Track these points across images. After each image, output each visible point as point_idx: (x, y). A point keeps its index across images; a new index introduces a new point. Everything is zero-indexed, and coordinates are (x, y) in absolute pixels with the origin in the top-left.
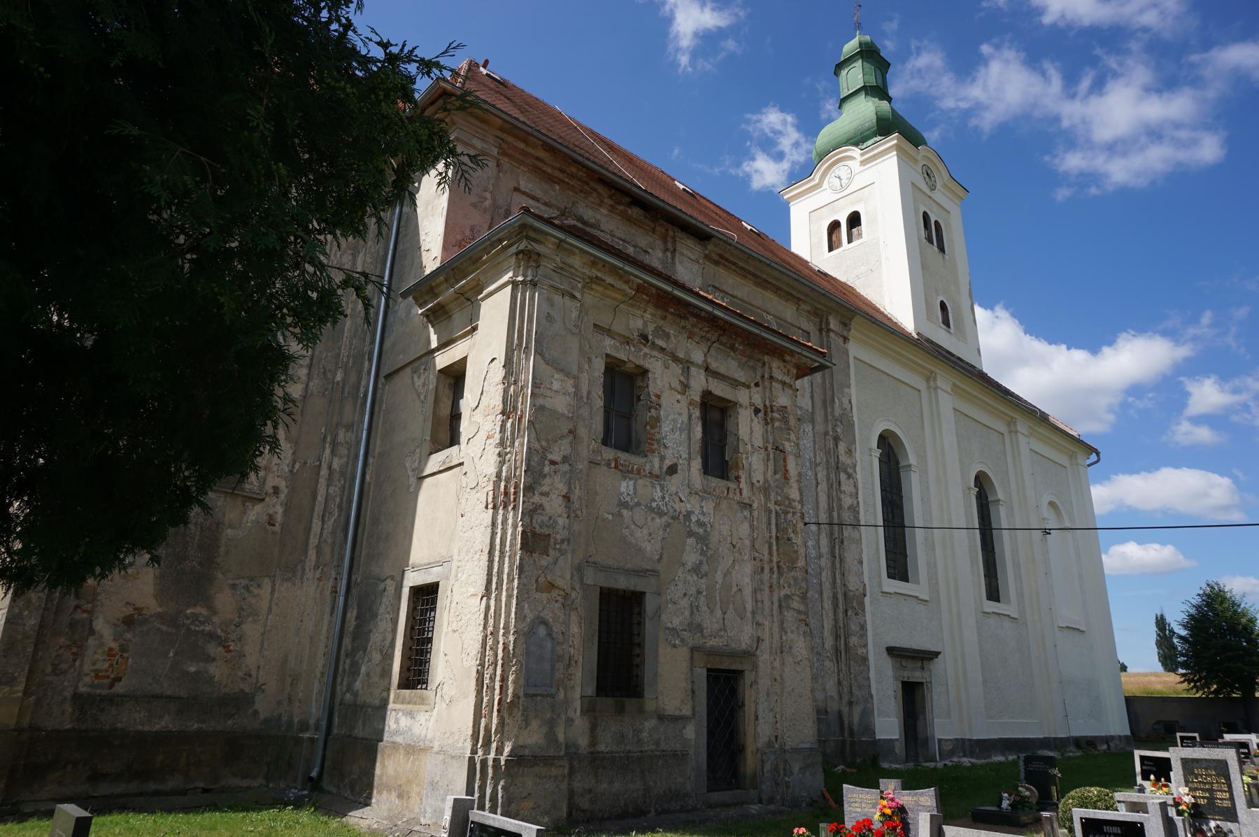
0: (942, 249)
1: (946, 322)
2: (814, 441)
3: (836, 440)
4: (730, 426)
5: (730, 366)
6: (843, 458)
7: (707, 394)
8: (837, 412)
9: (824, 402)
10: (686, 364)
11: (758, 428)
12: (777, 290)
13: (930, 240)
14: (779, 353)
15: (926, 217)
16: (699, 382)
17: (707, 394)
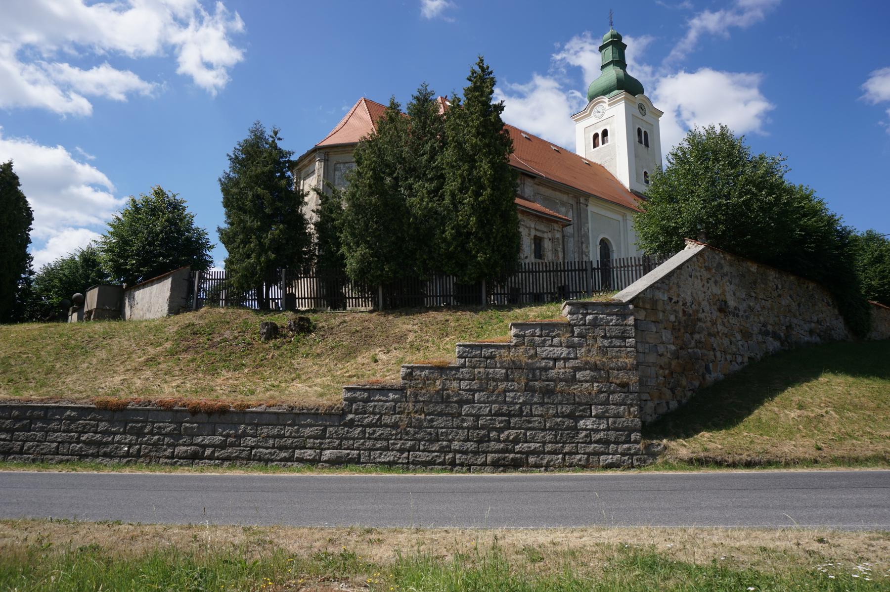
0: (647, 145)
2: (790, 296)
3: (582, 243)
5: (542, 227)
7: (535, 236)
10: (529, 228)
11: (550, 244)
12: (560, 191)
13: (640, 142)
14: (557, 222)
15: (639, 130)
16: (533, 233)
17: (535, 236)
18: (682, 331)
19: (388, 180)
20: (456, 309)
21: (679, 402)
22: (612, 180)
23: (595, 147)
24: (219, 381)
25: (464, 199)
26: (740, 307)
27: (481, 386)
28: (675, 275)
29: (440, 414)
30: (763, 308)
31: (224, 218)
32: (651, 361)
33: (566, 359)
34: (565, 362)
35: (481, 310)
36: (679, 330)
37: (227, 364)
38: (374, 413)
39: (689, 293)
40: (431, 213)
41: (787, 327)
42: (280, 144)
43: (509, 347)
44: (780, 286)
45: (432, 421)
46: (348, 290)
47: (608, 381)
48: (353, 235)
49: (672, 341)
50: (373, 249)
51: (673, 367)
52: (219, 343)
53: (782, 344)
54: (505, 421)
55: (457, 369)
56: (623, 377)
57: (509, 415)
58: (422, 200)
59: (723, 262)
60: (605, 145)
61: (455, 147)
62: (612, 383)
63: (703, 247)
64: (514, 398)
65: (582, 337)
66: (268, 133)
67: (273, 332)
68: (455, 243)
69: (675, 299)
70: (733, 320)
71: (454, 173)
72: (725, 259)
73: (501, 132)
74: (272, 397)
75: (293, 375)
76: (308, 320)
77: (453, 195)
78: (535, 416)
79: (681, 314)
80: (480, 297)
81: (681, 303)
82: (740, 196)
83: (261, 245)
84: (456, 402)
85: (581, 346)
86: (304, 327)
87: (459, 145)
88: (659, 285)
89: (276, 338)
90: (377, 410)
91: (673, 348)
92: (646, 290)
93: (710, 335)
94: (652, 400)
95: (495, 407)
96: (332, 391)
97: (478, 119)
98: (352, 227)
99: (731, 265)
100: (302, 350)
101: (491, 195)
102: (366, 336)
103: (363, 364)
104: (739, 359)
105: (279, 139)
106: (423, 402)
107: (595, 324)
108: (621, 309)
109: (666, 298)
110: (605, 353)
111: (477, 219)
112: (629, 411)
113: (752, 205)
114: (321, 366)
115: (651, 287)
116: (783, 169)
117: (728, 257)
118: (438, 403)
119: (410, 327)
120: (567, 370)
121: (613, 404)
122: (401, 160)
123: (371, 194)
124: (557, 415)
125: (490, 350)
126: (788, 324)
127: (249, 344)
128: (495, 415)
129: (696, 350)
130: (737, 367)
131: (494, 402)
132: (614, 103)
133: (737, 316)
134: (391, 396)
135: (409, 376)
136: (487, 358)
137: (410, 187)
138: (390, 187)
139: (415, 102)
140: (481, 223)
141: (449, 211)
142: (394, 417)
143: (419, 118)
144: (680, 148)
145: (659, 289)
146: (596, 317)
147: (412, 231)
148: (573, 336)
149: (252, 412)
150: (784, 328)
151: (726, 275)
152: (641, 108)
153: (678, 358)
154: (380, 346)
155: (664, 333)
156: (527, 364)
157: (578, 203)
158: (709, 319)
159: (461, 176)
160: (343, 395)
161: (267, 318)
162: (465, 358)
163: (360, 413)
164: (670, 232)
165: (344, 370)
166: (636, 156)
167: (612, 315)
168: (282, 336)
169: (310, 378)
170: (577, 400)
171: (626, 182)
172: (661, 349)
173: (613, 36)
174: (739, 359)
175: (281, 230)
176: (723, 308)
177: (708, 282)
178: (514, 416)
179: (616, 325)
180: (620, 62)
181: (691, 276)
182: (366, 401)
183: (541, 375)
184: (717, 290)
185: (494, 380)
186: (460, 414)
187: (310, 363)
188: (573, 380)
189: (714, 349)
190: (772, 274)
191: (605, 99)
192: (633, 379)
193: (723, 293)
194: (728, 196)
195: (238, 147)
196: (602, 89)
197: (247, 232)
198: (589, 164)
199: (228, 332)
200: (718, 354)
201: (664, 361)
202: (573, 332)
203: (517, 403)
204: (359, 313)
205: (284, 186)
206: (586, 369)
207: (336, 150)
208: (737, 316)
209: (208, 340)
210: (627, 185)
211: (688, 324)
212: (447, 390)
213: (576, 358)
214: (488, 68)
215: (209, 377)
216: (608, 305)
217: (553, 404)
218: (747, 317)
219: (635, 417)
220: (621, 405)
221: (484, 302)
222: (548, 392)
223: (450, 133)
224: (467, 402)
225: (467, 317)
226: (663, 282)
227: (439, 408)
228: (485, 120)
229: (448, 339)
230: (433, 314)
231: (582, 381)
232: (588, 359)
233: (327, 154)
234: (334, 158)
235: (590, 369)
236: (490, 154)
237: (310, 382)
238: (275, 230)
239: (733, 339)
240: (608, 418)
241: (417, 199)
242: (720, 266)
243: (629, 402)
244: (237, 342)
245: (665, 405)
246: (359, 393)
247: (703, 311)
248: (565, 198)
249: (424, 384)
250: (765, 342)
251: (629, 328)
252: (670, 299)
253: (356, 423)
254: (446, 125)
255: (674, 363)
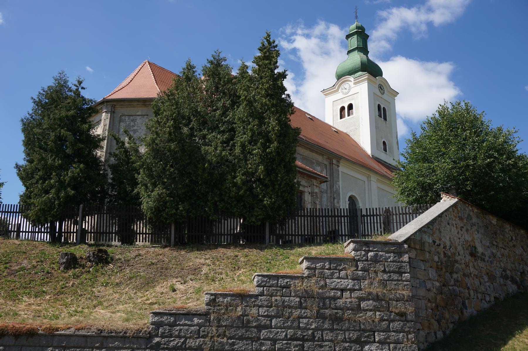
0: (385, 119)
1: (385, 150)
2: (522, 247)
3: (334, 198)
4: (303, 197)
6: (336, 204)
8: (335, 190)
9: (331, 186)
11: (310, 198)
12: (316, 152)
14: (315, 178)
15: (379, 106)
18: (444, 270)
19: (185, 130)
20: (243, 247)
21: (444, 333)
22: (356, 146)
23: (341, 118)
24: (22, 306)
25: (253, 150)
26: (486, 253)
27: (278, 313)
28: (437, 222)
29: (241, 338)
30: (503, 255)
31: (23, 155)
32: (421, 295)
33: (352, 290)
34: (351, 293)
35: (266, 248)
36: (442, 269)
37: (28, 291)
38: (179, 337)
39: (448, 238)
40: (222, 161)
41: (521, 273)
42: (83, 93)
43: (302, 278)
44: (514, 238)
45: (233, 344)
46: (139, 227)
47: (388, 311)
48: (151, 176)
49: (436, 278)
50: (168, 190)
51: (438, 301)
52: (17, 271)
53: (519, 287)
54: (300, 345)
55: (256, 296)
56: (400, 307)
57: (303, 339)
58: (216, 149)
59: (471, 213)
60: (349, 117)
61: (246, 105)
62: (392, 312)
63: (456, 200)
64: (307, 324)
65: (365, 271)
66: (72, 83)
67: (72, 262)
68: (245, 188)
69: (438, 242)
70: (481, 264)
71: (244, 128)
72: (473, 212)
73: (283, 96)
74: (78, 321)
75: (95, 302)
76: (106, 252)
77: (243, 146)
78: (326, 341)
79: (442, 256)
80: (264, 237)
81: (442, 246)
82: (485, 159)
83: (61, 182)
84: (255, 327)
85: (364, 279)
86: (102, 259)
87: (250, 103)
88: (426, 230)
89: (75, 268)
90: (182, 334)
91: (437, 284)
92: (416, 233)
93: (464, 275)
94: (423, 329)
95: (290, 332)
96: (136, 316)
97: (267, 83)
98: (149, 169)
99: (478, 217)
100: (101, 279)
101: (278, 148)
102: (162, 268)
103: (162, 293)
104: (488, 299)
105: (83, 88)
106: (225, 326)
107: (376, 260)
108: (397, 247)
109: (431, 241)
110: (385, 286)
111: (265, 167)
112: (408, 338)
113: (495, 167)
114: (122, 294)
115: (420, 230)
116: (517, 140)
117: (476, 210)
118: (238, 327)
119: (202, 261)
120: (353, 300)
121: (394, 331)
122: (196, 113)
123: (170, 140)
124: (344, 341)
125: (286, 281)
126: (522, 271)
127: (48, 273)
128: (290, 339)
129: (455, 288)
130: (486, 305)
131: (290, 327)
132: (359, 82)
133: (484, 261)
134: (196, 320)
135: (213, 301)
136: (283, 287)
137: (204, 137)
138: (187, 135)
139: (209, 65)
140: (268, 172)
141: (240, 160)
142: (198, 340)
143: (214, 78)
144: (434, 118)
145: (425, 232)
146: (377, 254)
147: (206, 175)
148: (357, 270)
149: (61, 335)
150: (519, 274)
151: (475, 225)
152: (381, 87)
153: (441, 293)
154: (177, 277)
155: (430, 270)
156: (318, 293)
157: (331, 164)
158: (463, 261)
159: (251, 130)
160: (151, 319)
161: (64, 250)
162: (264, 287)
163: (167, 337)
164: (426, 188)
165: (145, 298)
166: (377, 128)
167: (390, 252)
168: (81, 266)
169: (112, 305)
170: (362, 327)
171: (368, 150)
172: (429, 285)
173: (357, 27)
174: (488, 299)
175: (81, 170)
176: (473, 254)
177: (461, 230)
178: (307, 340)
179: (393, 262)
180: (363, 49)
181: (449, 224)
182: (172, 325)
183: (330, 304)
184: (468, 238)
185: (290, 307)
186: (259, 338)
187: (111, 292)
188: (358, 309)
189: (468, 288)
190: (508, 227)
191: (351, 78)
192: (410, 309)
193: (473, 240)
194: (475, 158)
195: (42, 92)
196: (348, 70)
197: (48, 171)
198: (337, 132)
199: (26, 261)
200: (472, 292)
201: (431, 295)
202: (357, 266)
203: (309, 329)
204: (144, 248)
205: (85, 129)
206: (369, 300)
207: (122, 103)
208: (484, 261)
209: (6, 268)
210: (369, 152)
211: (447, 265)
212: (247, 315)
213: (360, 289)
214: (274, 42)
215: (11, 303)
216: (387, 243)
217: (341, 330)
218: (491, 262)
219: (413, 343)
220: (400, 332)
221: (267, 241)
222: (337, 319)
223: (241, 93)
224: (265, 327)
225: (254, 254)
226: (429, 228)
227: (240, 332)
228: (273, 84)
229: (240, 272)
230: (222, 250)
231: (367, 310)
232: (371, 290)
233: (114, 107)
234: (120, 111)
235: (373, 300)
236: (277, 113)
237: (112, 309)
238: (75, 170)
239: (482, 281)
240: (389, 343)
241: (212, 148)
242: (469, 217)
243: (407, 329)
244: (36, 271)
245: (433, 334)
246: (165, 317)
247: (459, 255)
248: (320, 158)
249: (227, 309)
250: (506, 285)
251: (404, 264)
252: (434, 242)
253: (162, 346)
254: (238, 86)
255: (439, 297)
